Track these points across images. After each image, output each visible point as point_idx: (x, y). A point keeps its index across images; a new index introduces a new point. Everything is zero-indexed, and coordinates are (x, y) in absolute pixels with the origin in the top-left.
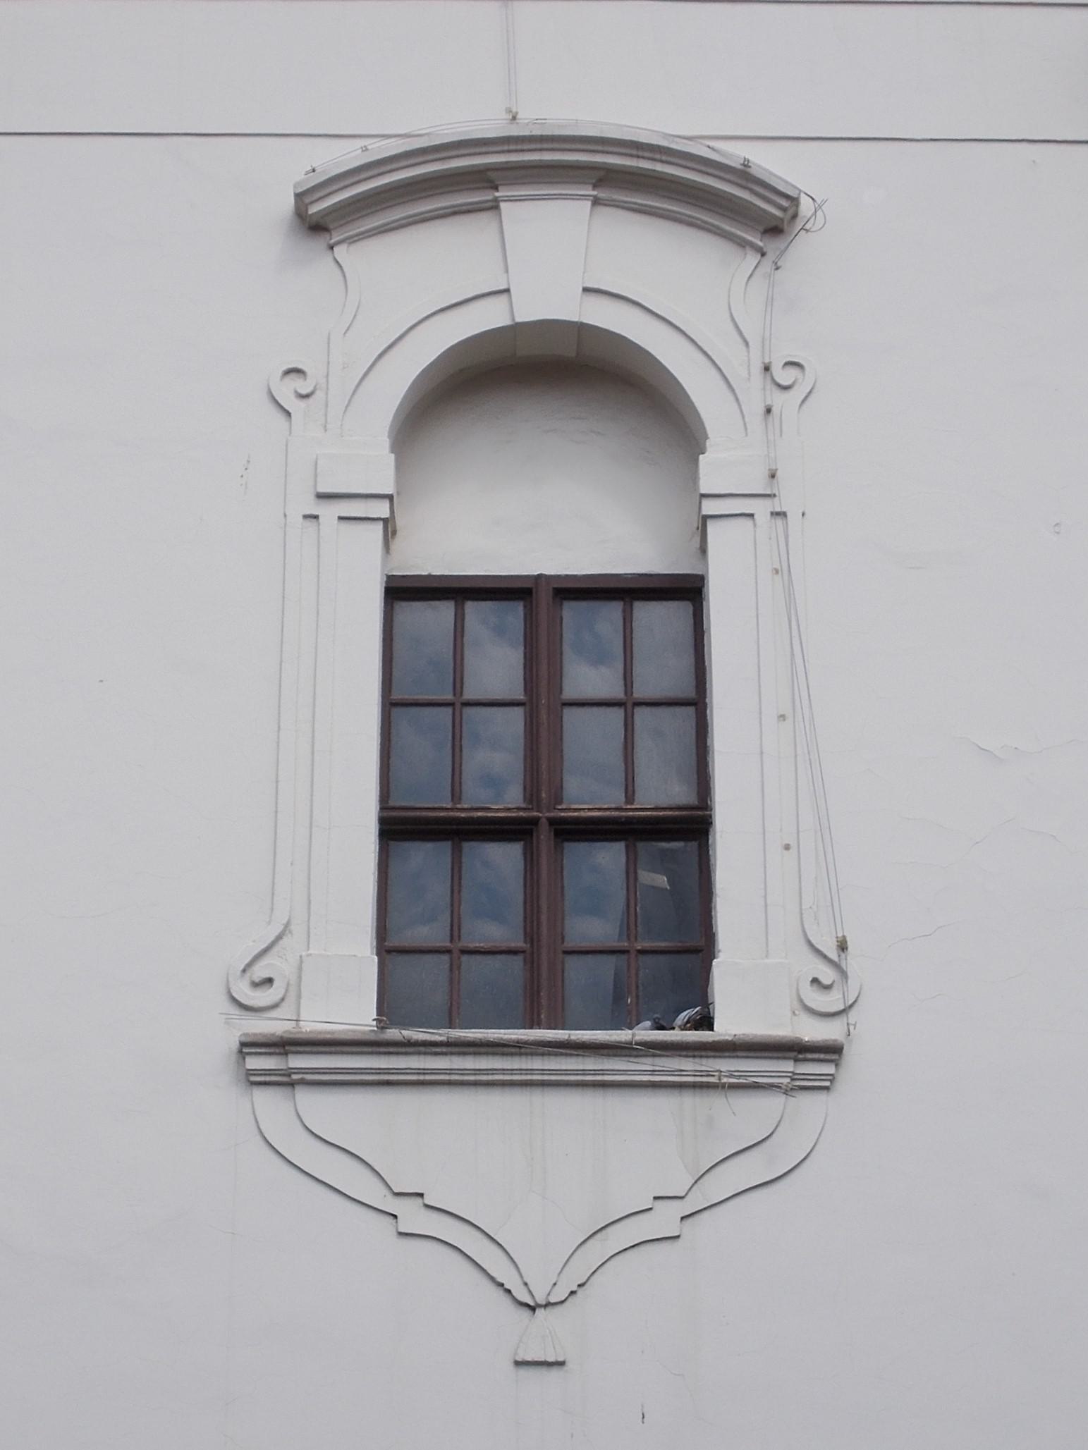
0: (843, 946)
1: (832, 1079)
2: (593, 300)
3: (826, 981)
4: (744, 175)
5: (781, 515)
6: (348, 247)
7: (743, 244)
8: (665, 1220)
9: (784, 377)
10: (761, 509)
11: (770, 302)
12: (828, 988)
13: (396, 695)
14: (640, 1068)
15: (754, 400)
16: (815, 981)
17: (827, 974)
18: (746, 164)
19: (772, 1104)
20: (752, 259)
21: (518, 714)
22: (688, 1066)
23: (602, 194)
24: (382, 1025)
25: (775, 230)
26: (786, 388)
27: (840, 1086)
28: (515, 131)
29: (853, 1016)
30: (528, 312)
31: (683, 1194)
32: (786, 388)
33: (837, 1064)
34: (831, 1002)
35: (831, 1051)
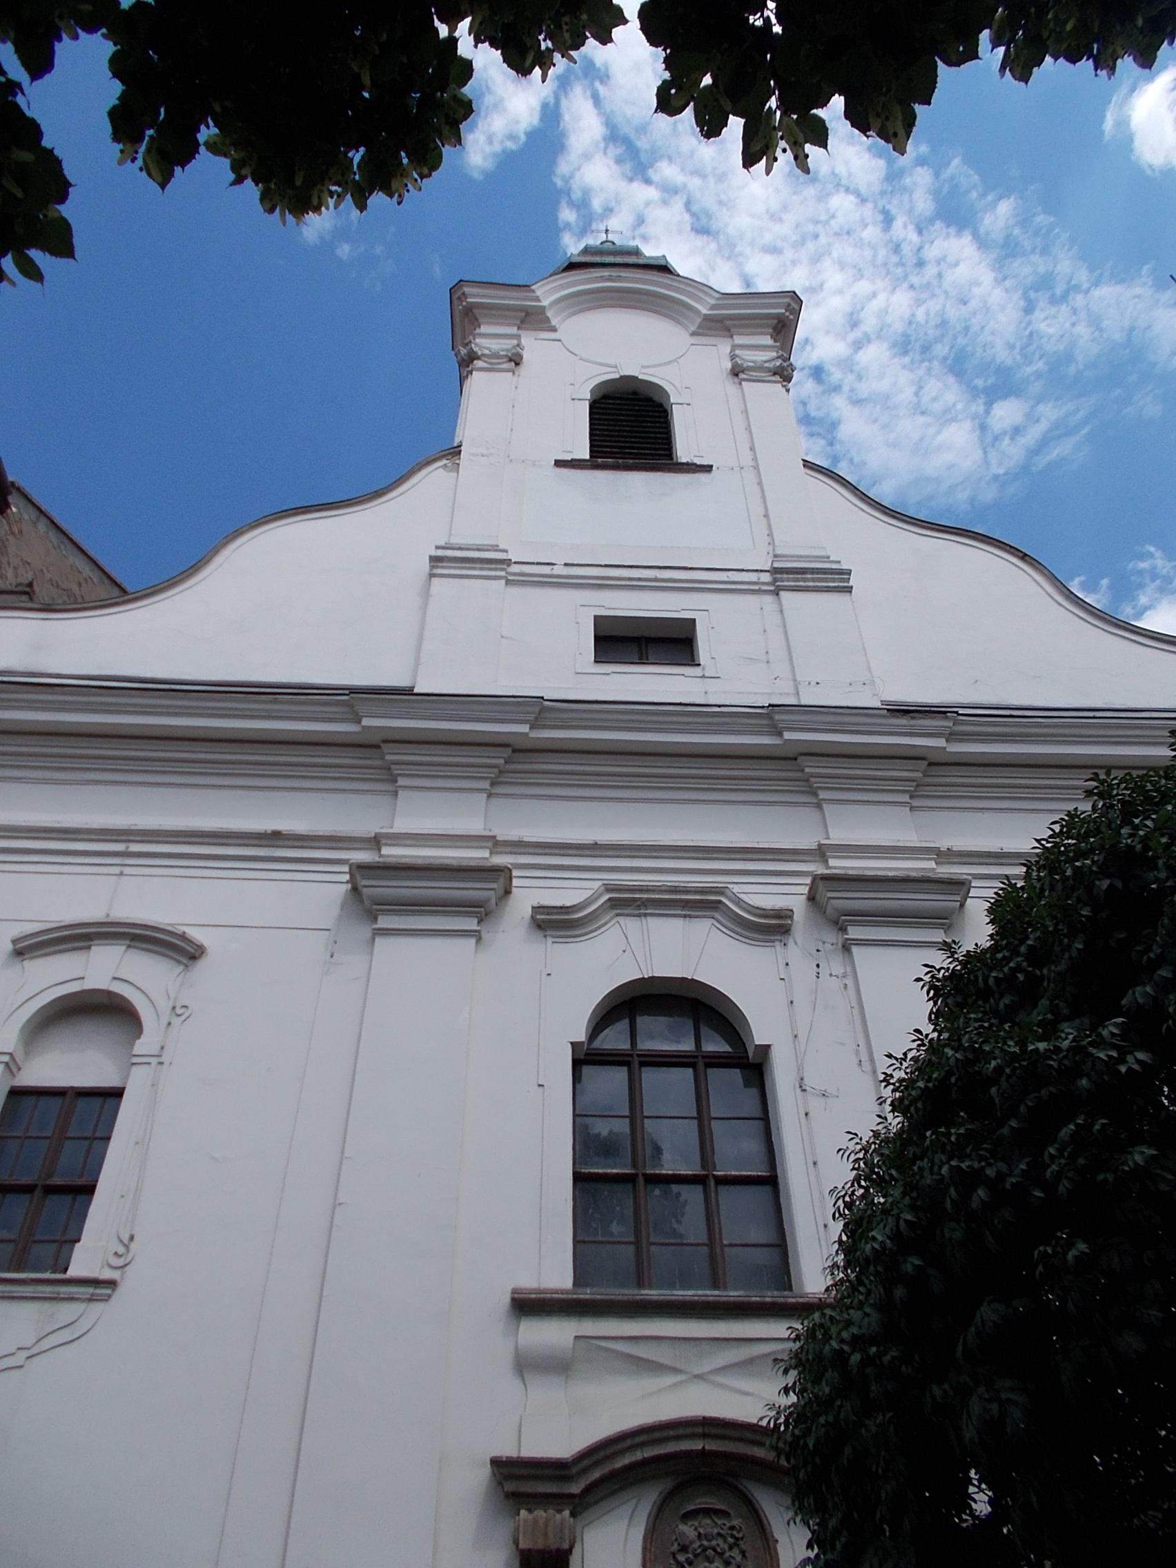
0: (132, 1238)
1: (110, 1296)
2: (117, 982)
3: (120, 1253)
4: (183, 937)
5: (161, 1063)
6: (125, 951)
7: (179, 962)
8: (20, 1358)
9: (179, 1011)
10: (154, 1061)
11: (182, 984)
12: (121, 1256)
13: (577, 1112)
14: (28, 1290)
15: (165, 1016)
16: (116, 1253)
17: (121, 1250)
18: (184, 933)
19: (78, 1307)
20: (181, 968)
21: (627, 1120)
22: (48, 1290)
23: (133, 944)
24: (580, 1277)
25: (193, 958)
26: (179, 1015)
27: (113, 1298)
28: (109, 920)
29: (127, 1268)
30: (88, 985)
31: (29, 1346)
32: (179, 1015)
33: (114, 1290)
34: (120, 1262)
35: (112, 1284)
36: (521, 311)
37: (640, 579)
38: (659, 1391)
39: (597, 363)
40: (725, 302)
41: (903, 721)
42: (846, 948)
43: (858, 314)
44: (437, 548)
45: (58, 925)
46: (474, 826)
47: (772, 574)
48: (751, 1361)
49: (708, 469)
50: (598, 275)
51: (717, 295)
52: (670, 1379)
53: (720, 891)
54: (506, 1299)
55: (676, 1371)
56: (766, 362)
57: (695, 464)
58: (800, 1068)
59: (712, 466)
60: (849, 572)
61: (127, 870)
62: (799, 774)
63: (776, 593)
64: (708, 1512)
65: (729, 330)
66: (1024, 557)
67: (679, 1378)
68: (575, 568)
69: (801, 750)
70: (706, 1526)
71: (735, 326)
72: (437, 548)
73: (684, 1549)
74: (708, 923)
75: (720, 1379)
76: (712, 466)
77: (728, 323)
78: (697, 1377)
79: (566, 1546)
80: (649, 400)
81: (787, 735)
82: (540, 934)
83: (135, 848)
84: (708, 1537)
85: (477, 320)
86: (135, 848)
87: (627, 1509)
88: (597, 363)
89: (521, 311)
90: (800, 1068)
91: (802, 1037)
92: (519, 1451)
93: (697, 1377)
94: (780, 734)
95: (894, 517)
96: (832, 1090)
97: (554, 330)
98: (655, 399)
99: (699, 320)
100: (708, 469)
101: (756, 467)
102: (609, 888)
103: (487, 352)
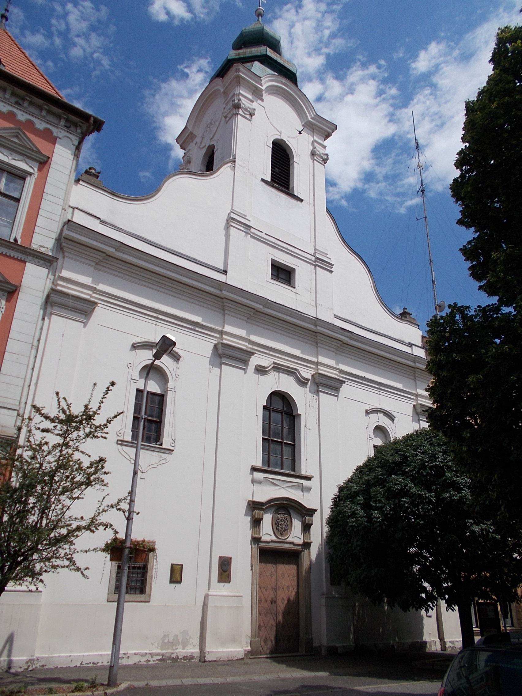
17: (173, 442)
35: (173, 451)
36: (255, 87)
37: (283, 247)
38: (276, 490)
39: (276, 129)
40: (316, 118)
41: (342, 331)
42: (318, 392)
43: (324, 29)
44: (336, 316)
45: (149, 341)
46: (87, 280)
47: (315, 259)
48: (292, 486)
49: (301, 200)
50: (281, 80)
51: (315, 114)
52: (279, 487)
53: (296, 370)
54: (250, 467)
55: (279, 486)
56: (323, 154)
57: (299, 198)
58: (306, 422)
59: (303, 200)
60: (333, 265)
61: (158, 324)
62: (315, 338)
63: (315, 266)
64: (283, 514)
65: (313, 129)
66: (369, 271)
67: (280, 487)
68: (268, 236)
69: (319, 332)
70: (282, 516)
71: (316, 130)
72: (336, 316)
73: (278, 519)
74: (292, 377)
75: (286, 489)
76: (303, 200)
77: (314, 127)
78: (283, 488)
79: (261, 517)
80: (288, 155)
81: (318, 328)
82: (257, 372)
83: (160, 316)
84: (282, 518)
85: (240, 83)
86: (160, 316)
87: (270, 511)
88: (276, 129)
89: (255, 87)
90: (306, 422)
91: (307, 414)
92: (253, 498)
93: (283, 488)
94: (316, 326)
95: (344, 243)
96: (311, 429)
97: (262, 100)
98: (287, 151)
99: (306, 121)
100: (301, 200)
101: (314, 205)
102: (274, 363)
103: (244, 106)
